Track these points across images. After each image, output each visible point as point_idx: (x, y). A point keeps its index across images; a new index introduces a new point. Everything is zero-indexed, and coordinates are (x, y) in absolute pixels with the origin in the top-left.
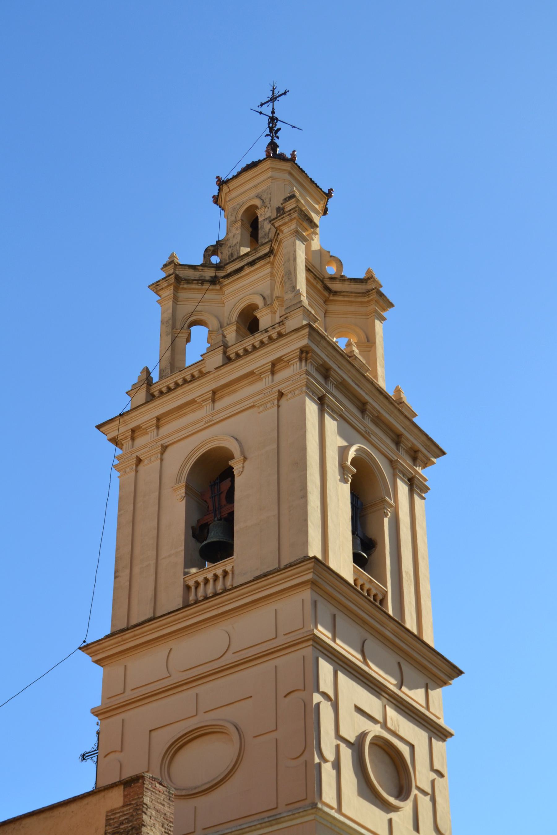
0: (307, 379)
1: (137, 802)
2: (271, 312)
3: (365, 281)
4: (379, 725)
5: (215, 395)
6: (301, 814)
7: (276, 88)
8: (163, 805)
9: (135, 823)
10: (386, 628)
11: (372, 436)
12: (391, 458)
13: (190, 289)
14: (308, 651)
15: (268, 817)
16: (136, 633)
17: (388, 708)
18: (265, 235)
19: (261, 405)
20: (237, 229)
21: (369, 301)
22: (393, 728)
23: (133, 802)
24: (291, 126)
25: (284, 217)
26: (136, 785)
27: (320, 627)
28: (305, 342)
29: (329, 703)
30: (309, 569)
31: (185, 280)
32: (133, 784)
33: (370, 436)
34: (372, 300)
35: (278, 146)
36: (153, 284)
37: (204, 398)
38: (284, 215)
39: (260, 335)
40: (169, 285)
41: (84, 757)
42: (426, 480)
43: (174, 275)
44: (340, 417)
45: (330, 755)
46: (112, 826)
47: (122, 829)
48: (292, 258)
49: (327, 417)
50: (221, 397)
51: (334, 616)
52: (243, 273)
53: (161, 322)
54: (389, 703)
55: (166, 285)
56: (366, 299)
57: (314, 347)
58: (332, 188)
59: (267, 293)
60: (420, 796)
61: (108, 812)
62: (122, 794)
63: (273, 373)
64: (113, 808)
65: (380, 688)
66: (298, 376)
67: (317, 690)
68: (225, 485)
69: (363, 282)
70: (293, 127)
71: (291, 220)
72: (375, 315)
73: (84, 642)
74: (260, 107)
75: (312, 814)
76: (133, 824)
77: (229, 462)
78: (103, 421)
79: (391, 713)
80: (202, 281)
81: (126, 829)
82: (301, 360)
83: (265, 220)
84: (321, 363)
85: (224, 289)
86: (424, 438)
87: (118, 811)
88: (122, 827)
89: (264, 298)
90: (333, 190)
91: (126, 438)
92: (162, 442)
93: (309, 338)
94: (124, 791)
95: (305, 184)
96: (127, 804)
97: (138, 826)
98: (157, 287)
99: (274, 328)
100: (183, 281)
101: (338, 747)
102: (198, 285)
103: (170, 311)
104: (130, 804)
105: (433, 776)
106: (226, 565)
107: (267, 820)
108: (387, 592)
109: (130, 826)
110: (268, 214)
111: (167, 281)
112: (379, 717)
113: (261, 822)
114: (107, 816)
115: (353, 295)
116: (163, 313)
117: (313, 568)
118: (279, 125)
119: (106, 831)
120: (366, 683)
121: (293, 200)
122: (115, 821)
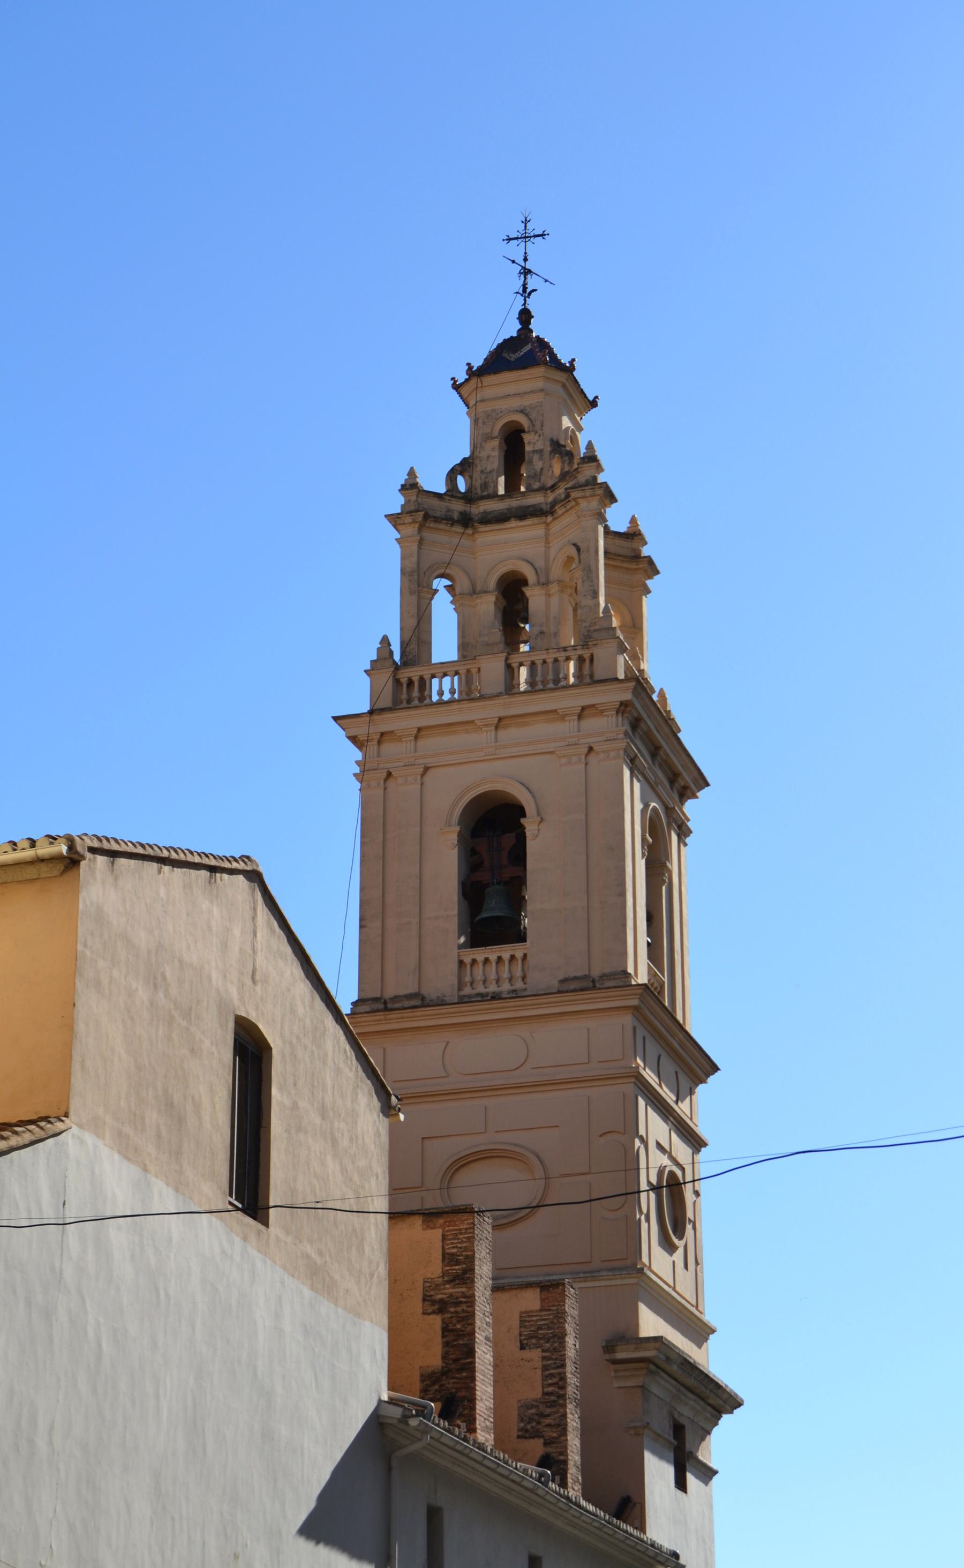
0: (628, 743)
1: (558, 1309)
2: (546, 594)
3: (631, 537)
5: (500, 723)
6: (623, 1276)
7: (529, 221)
9: (557, 1331)
10: (674, 1039)
11: (659, 787)
12: (667, 803)
13: (436, 529)
15: (584, 1273)
16: (405, 1015)
18: (535, 474)
19: (564, 756)
21: (636, 569)
24: (543, 280)
25: (584, 490)
26: (555, 1290)
28: (628, 696)
30: (635, 994)
31: (434, 517)
32: (551, 1289)
33: (657, 786)
34: (640, 569)
35: (533, 317)
37: (486, 723)
38: (586, 488)
39: (555, 652)
40: (414, 522)
42: (688, 820)
43: (423, 512)
46: (528, 1329)
47: (541, 1334)
52: (507, 525)
53: (401, 570)
55: (411, 521)
56: (634, 566)
58: (598, 395)
59: (540, 564)
61: (521, 1313)
62: (539, 1297)
63: (580, 717)
64: (528, 1310)
68: (509, 840)
69: (628, 538)
72: (642, 590)
74: (506, 242)
75: (636, 1277)
76: (555, 1332)
77: (521, 819)
81: (545, 1335)
82: (617, 713)
83: (535, 452)
85: (477, 536)
86: (696, 774)
90: (599, 397)
92: (425, 761)
94: (541, 1294)
95: (576, 398)
96: (545, 1308)
97: (560, 1335)
98: (396, 519)
99: (575, 649)
100: (430, 519)
102: (447, 526)
103: (415, 559)
104: (549, 1310)
107: (582, 1275)
108: (664, 982)
109: (550, 1333)
110: (539, 446)
111: (412, 516)
114: (520, 1317)
115: (621, 558)
116: (403, 558)
117: (641, 994)
118: (532, 283)
119: (520, 1332)
120: (662, 1112)
121: (595, 464)
122: (531, 1323)
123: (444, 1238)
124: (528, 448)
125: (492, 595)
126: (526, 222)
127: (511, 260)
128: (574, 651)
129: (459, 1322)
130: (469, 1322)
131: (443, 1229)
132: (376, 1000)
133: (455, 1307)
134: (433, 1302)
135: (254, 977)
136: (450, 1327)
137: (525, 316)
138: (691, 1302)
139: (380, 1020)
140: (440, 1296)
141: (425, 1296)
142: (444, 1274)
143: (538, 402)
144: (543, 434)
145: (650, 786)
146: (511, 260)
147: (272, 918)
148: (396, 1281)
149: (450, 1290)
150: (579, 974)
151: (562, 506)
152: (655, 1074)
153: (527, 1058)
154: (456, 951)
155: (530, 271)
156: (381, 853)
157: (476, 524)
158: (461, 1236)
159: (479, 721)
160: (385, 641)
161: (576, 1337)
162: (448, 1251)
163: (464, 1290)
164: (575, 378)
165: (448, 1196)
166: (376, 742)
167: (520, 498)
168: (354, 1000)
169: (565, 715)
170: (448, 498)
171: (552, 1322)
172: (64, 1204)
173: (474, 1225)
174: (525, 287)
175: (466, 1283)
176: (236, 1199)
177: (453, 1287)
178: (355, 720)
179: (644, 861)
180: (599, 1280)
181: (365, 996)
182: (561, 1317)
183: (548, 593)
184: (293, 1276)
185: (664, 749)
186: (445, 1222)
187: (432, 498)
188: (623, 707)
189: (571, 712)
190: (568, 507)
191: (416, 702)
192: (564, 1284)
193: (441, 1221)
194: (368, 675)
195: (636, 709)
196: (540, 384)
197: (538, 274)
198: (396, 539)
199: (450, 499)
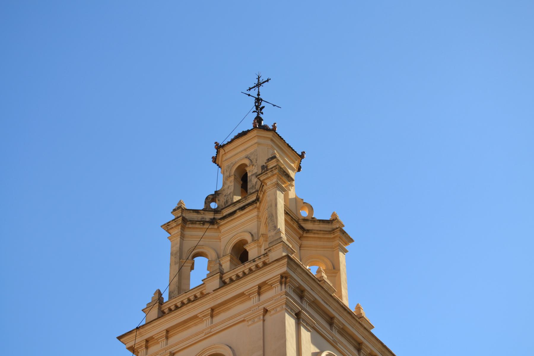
0: (287, 298)
7: (260, 77)
11: (339, 344)
13: (193, 228)
18: (253, 186)
20: (231, 182)
21: (334, 238)
24: (272, 105)
25: (267, 173)
28: (284, 269)
31: (190, 221)
33: (337, 344)
36: (165, 224)
38: (268, 172)
39: (249, 264)
40: (178, 225)
52: (236, 216)
53: (171, 254)
55: (175, 225)
56: (332, 236)
59: (254, 231)
63: (259, 294)
69: (329, 223)
70: (274, 106)
71: (273, 175)
74: (249, 91)
80: (204, 222)
82: (281, 283)
85: (221, 228)
86: (379, 345)
89: (252, 235)
91: (141, 347)
93: (287, 266)
98: (168, 227)
99: (260, 259)
100: (188, 222)
102: (201, 225)
103: (178, 245)
111: (175, 222)
121: (275, 160)
125: (228, 256)
127: (251, 96)
128: (260, 260)
143: (255, 150)
144: (257, 165)
146: (251, 96)
151: (261, 191)
159: (200, 314)
160: (159, 293)
166: (144, 347)
167: (244, 201)
169: (249, 294)
170: (203, 212)
183: (259, 245)
187: (192, 213)
188: (284, 278)
189: (253, 291)
194: (144, 312)
196: (256, 140)
197: (268, 102)
199: (204, 212)
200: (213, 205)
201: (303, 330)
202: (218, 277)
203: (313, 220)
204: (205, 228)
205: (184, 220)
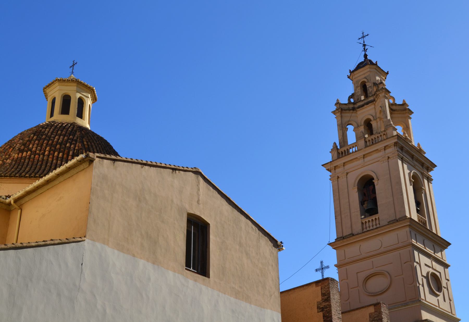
0: (398, 153)
4: (431, 268)
5: (364, 156)
8: (386, 311)
11: (416, 166)
14: (410, 248)
15: (404, 304)
16: (348, 239)
17: (433, 262)
18: (370, 92)
20: (359, 89)
21: (406, 113)
22: (435, 268)
23: (378, 311)
27: (413, 240)
28: (396, 140)
29: (418, 265)
31: (344, 109)
34: (407, 112)
35: (367, 56)
36: (333, 111)
40: (339, 112)
41: (316, 270)
42: (431, 176)
44: (408, 163)
45: (421, 283)
48: (384, 106)
49: (404, 164)
50: (366, 157)
51: (416, 234)
52: (364, 107)
53: (337, 125)
54: (433, 260)
56: (405, 112)
57: (399, 142)
59: (374, 115)
60: (444, 289)
61: (369, 314)
62: (374, 308)
63: (385, 150)
65: (430, 256)
66: (394, 152)
67: (415, 261)
68: (371, 187)
69: (402, 105)
70: (371, 47)
71: (382, 92)
73: (329, 242)
78: (324, 163)
79: (434, 263)
80: (350, 110)
82: (394, 146)
84: (401, 146)
85: (357, 112)
86: (431, 163)
87: (373, 313)
88: (375, 319)
89: (373, 117)
91: (332, 169)
93: (397, 139)
101: (422, 279)
103: (340, 121)
104: (377, 312)
105: (447, 281)
106: (376, 216)
107: (404, 305)
108: (426, 220)
110: (370, 85)
112: (431, 266)
113: (402, 305)
114: (369, 315)
116: (338, 122)
117: (410, 221)
118: (366, 48)
121: (382, 84)
123: (321, 289)
124: (367, 87)
126: (363, 33)
129: (327, 313)
130: (330, 313)
131: (321, 286)
132: (341, 237)
133: (326, 309)
134: (320, 308)
135: (199, 202)
136: (325, 315)
137: (366, 56)
138: (448, 311)
139: (342, 242)
140: (322, 306)
141: (318, 307)
142: (322, 299)
145: (411, 166)
147: (209, 186)
148: (309, 304)
149: (324, 304)
150: (393, 219)
152: (422, 245)
153: (381, 246)
154: (360, 220)
155: (365, 45)
156: (338, 198)
157: (356, 109)
158: (326, 287)
160: (335, 143)
161: (388, 319)
162: (323, 292)
163: (328, 303)
164: (378, 66)
165: (366, 289)
168: (336, 239)
171: (378, 315)
172: (82, 264)
173: (329, 283)
174: (364, 49)
175: (328, 301)
176: (192, 269)
177: (325, 303)
178: (327, 165)
179: (412, 187)
180: (409, 305)
181: (338, 237)
182: (380, 313)
184: (225, 294)
185: (415, 156)
186: (321, 284)
188: (396, 144)
190: (378, 97)
191: (341, 156)
192: (380, 303)
193: (320, 284)
195: (400, 144)
196: (369, 70)
198: (335, 117)
200: (352, 100)
201: (404, 164)
202: (364, 140)
203: (395, 104)
204: (351, 112)
205: (342, 110)
